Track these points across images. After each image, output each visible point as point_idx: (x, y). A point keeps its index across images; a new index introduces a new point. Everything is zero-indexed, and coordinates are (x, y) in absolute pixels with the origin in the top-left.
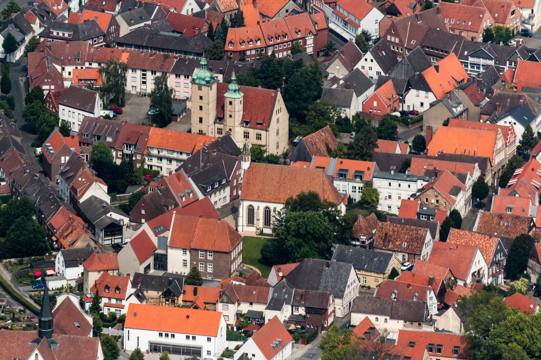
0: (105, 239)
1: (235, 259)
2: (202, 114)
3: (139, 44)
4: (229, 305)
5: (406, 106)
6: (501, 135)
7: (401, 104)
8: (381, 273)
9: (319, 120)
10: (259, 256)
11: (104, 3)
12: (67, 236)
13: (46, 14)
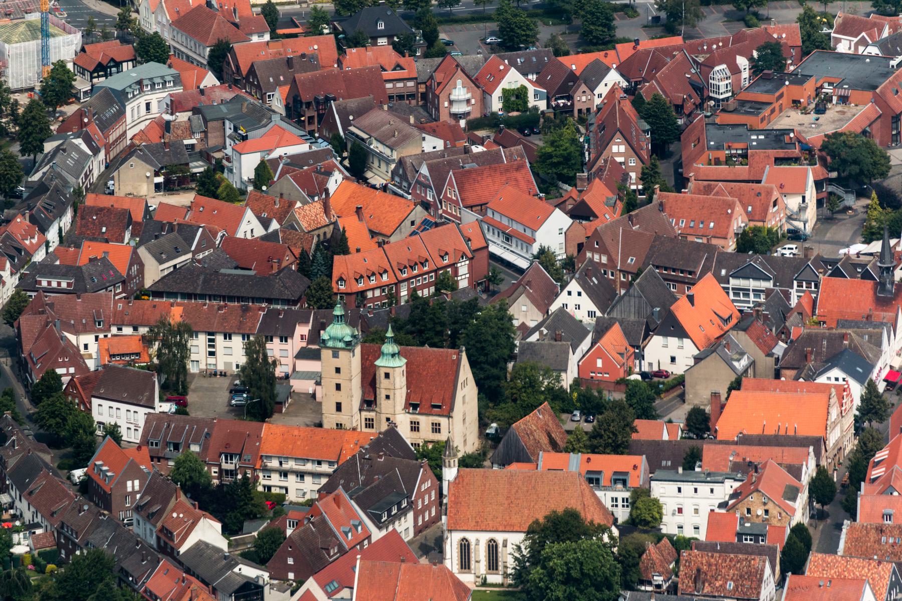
3: (189, 291)
5: (647, 365)
7: (637, 362)
11: (104, 229)
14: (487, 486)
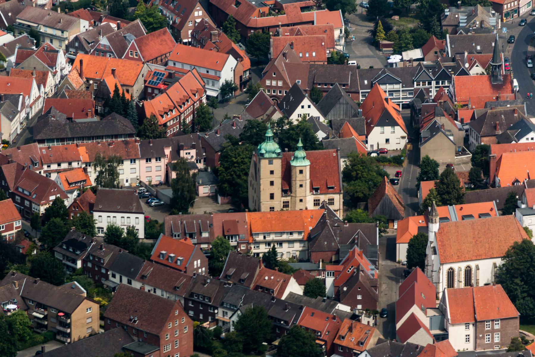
3: (62, 136)
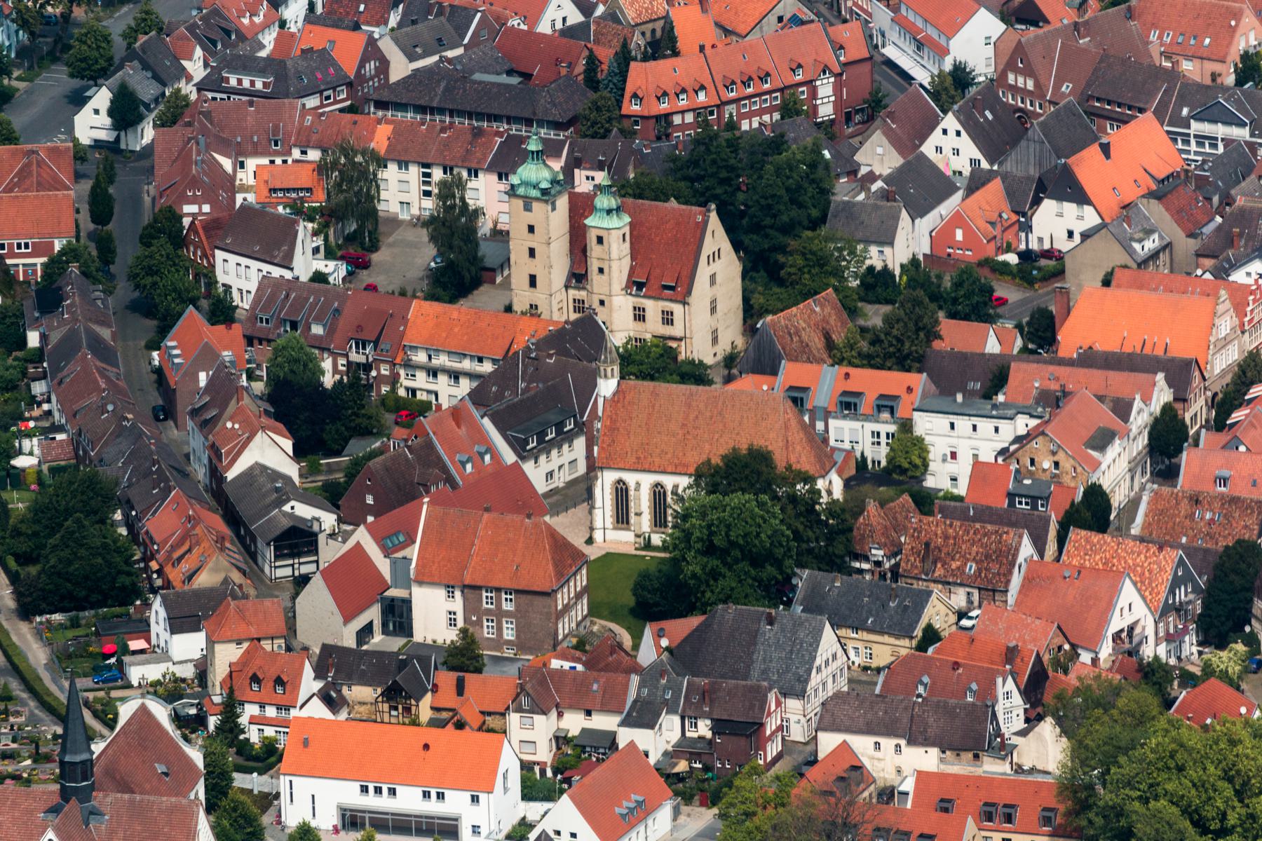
0: (277, 564)
1: (567, 608)
2: (535, 267)
3: (422, 102)
4: (536, 717)
5: (1036, 241)
6: (1228, 304)
7: (1023, 235)
8: (904, 637)
9: (812, 276)
10: (630, 600)
11: (362, 8)
12: (180, 559)
13: (221, 36)
14: (657, 408)
